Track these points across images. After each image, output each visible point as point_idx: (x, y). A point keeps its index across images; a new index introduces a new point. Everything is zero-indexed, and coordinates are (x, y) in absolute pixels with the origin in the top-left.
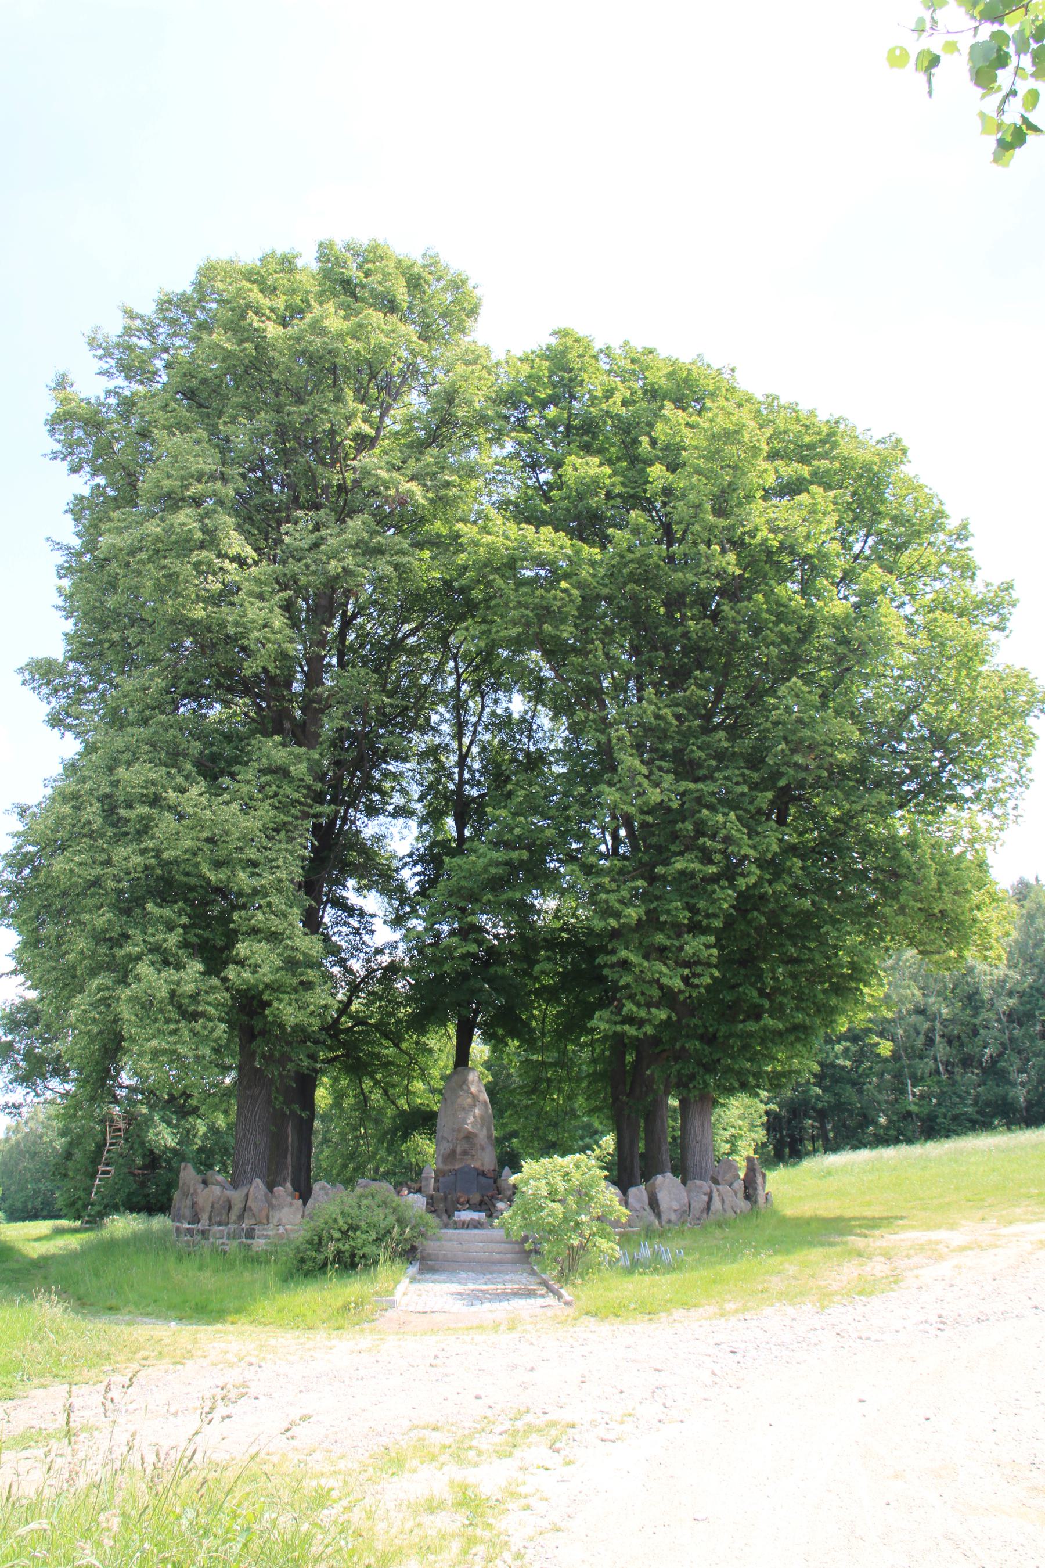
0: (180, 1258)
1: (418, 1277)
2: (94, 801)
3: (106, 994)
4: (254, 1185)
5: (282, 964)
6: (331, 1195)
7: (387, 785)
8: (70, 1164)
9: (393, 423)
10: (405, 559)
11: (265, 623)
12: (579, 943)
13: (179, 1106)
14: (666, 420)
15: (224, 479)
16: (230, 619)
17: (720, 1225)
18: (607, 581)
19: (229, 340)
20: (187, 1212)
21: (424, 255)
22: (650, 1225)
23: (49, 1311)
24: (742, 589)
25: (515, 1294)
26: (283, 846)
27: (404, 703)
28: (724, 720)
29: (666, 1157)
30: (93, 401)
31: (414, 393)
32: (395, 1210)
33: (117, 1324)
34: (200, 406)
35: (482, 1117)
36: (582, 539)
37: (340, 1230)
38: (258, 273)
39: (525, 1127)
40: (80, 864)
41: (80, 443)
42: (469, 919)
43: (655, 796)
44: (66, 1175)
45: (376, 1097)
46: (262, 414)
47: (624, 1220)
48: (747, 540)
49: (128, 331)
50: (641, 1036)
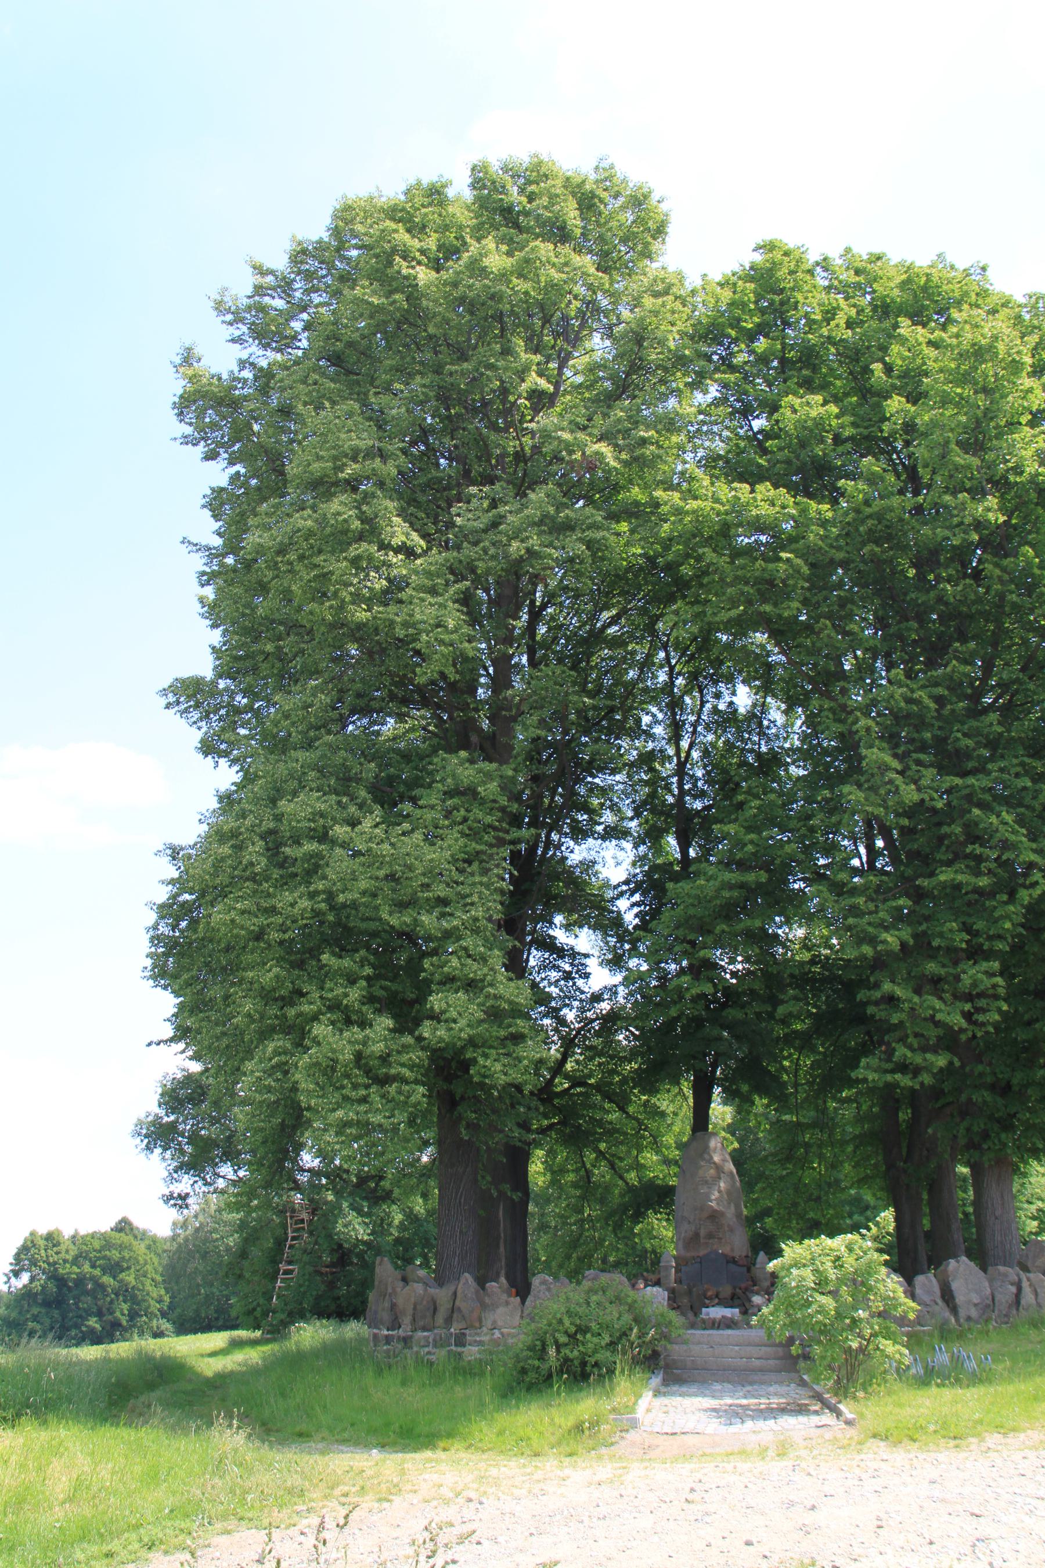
0: (379, 1372)
1: (663, 1389)
2: (256, 839)
3: (283, 1058)
4: (462, 1281)
5: (482, 1016)
6: (554, 1291)
7: (595, 802)
8: (246, 1263)
9: (572, 377)
10: (599, 535)
11: (439, 622)
12: (833, 979)
13: (370, 1191)
14: (903, 340)
15: (383, 455)
16: (398, 619)
17: (1035, 1324)
18: (842, 542)
19: (374, 293)
20: (385, 1316)
21: (597, 168)
22: (946, 1322)
23: (230, 1440)
24: (1009, 538)
25: (783, 1410)
26: (477, 879)
27: (609, 703)
28: (996, 700)
29: (958, 1236)
30: (225, 376)
31: (597, 338)
32: (631, 1307)
33: (310, 1453)
34: (349, 372)
35: (729, 1193)
36: (810, 496)
37: (566, 1332)
38: (403, 210)
39: (780, 1203)
40: (243, 912)
41: (214, 426)
42: (702, 953)
43: (910, 794)
44: (240, 1276)
45: (601, 1172)
46: (418, 378)
47: (912, 1316)
48: (1012, 478)
49: (259, 290)
50: (917, 1087)
